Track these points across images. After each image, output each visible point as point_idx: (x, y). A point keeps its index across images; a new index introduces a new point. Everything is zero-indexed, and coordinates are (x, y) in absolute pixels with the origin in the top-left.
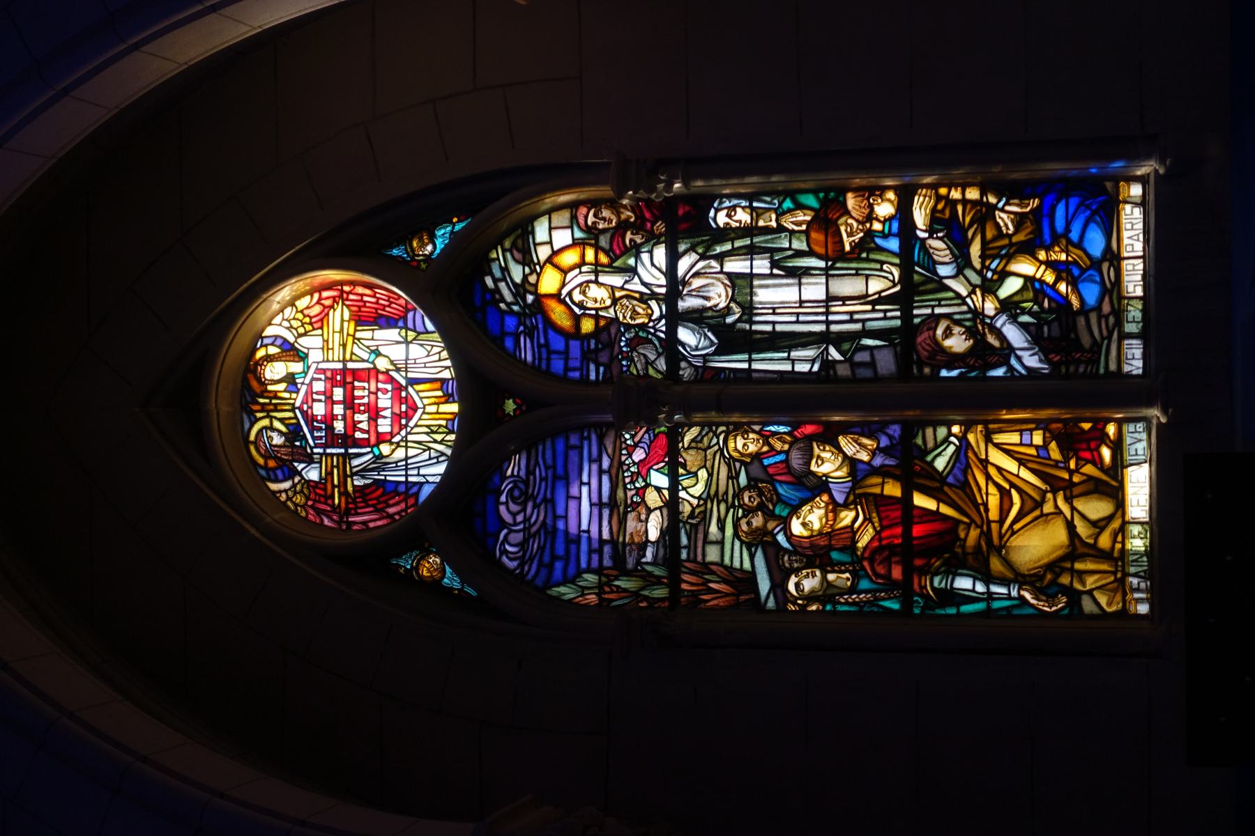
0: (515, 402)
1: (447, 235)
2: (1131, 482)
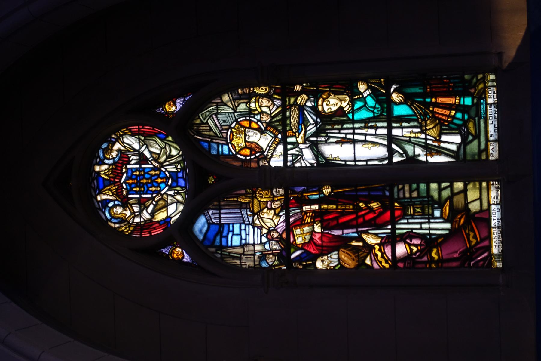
0: (213, 178)
1: (181, 102)
2: (493, 215)
